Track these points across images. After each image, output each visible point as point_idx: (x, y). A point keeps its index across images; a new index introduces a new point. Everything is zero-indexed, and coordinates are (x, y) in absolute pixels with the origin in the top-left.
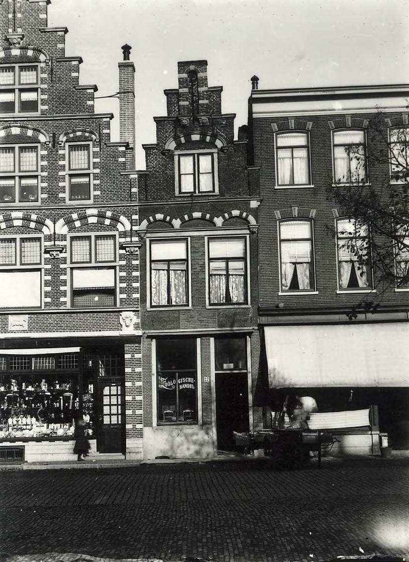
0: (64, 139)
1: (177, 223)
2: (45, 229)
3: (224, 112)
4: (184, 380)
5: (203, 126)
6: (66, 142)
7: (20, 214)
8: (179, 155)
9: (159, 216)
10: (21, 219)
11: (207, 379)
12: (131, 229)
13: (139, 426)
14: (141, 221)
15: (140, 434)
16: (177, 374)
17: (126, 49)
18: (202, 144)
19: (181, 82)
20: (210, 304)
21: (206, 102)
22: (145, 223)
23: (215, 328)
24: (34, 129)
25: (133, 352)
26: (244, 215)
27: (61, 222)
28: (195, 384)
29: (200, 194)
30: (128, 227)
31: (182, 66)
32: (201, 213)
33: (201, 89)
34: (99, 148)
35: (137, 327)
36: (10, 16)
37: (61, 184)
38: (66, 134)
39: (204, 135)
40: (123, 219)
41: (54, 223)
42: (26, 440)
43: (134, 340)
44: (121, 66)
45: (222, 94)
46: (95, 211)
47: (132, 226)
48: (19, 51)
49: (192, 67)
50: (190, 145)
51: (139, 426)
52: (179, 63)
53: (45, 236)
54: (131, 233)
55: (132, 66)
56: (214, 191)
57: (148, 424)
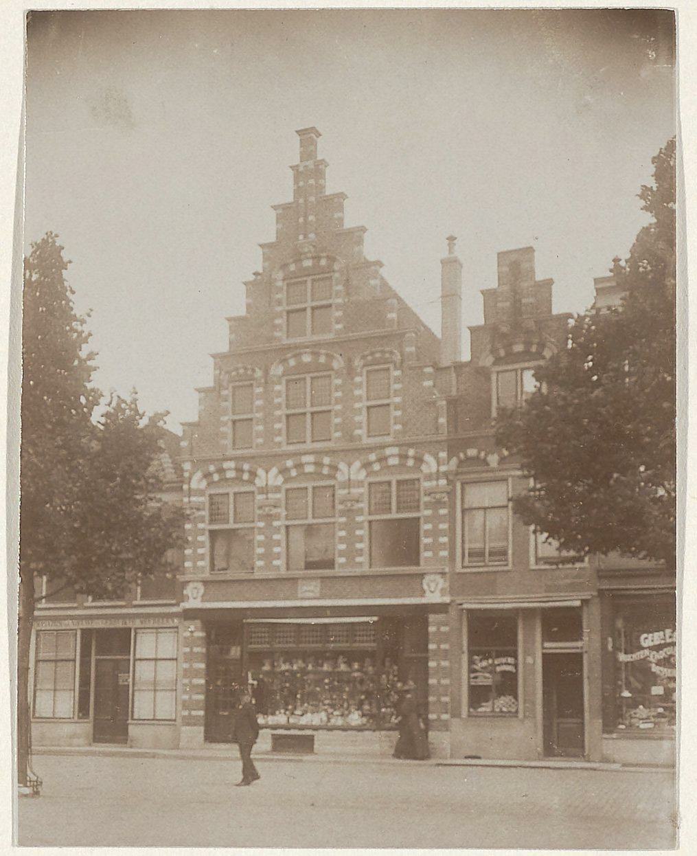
0: (362, 362)
1: (493, 460)
2: (338, 475)
3: (555, 312)
4: (504, 660)
5: (528, 332)
6: (364, 366)
7: (310, 458)
9: (472, 452)
11: (530, 660)
13: (445, 717)
14: (449, 458)
15: (445, 726)
16: (494, 654)
17: (451, 239)
20: (538, 560)
21: (531, 300)
22: (454, 461)
23: (541, 593)
24: (295, 356)
25: (439, 624)
26: (462, 455)
27: (274, 471)
28: (516, 666)
30: (434, 469)
32: (199, 471)
33: (525, 285)
34: (222, 393)
35: (443, 592)
36: (301, 220)
37: (357, 419)
38: (364, 357)
40: (428, 458)
41: (267, 473)
42: (316, 729)
43: (441, 608)
44: (444, 262)
45: (554, 287)
46: (395, 450)
47: (438, 465)
48: (311, 261)
49: (513, 257)
51: (445, 717)
52: (499, 254)
53: (258, 488)
54: (438, 475)
55: (456, 261)
57: (456, 714)
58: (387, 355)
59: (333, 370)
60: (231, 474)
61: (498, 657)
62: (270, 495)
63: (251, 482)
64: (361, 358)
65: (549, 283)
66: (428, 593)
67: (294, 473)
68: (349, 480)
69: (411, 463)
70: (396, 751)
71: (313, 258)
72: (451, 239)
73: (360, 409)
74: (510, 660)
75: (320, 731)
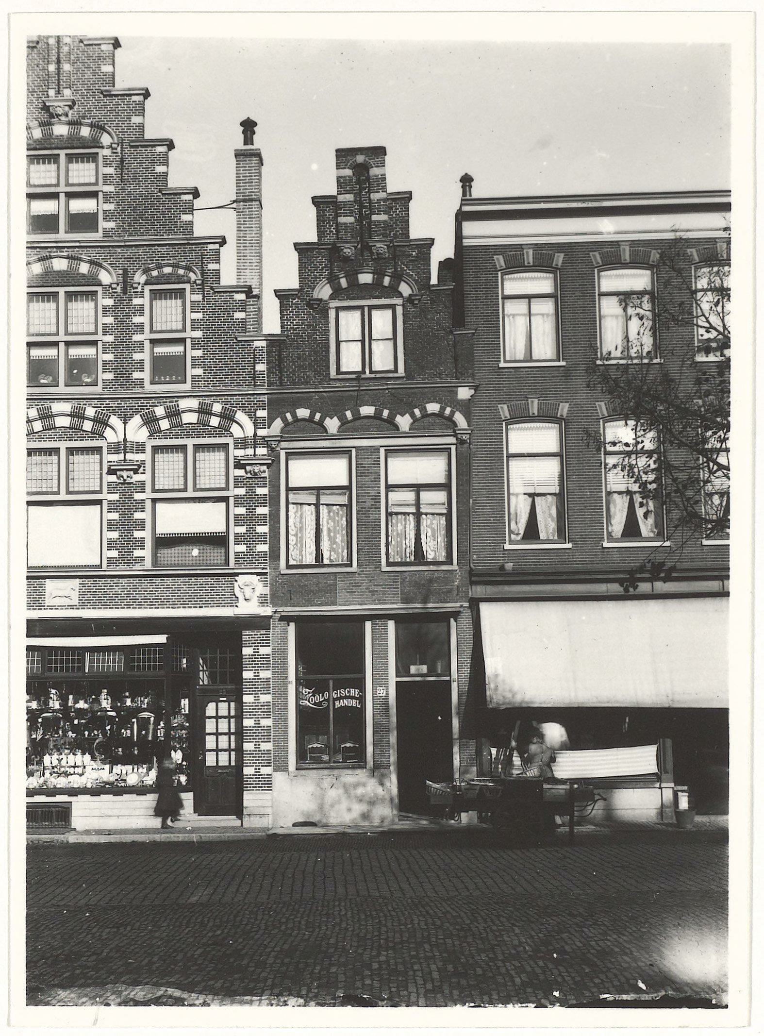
1: (332, 424)
2: (108, 433)
4: (344, 692)
5: (379, 258)
6: (146, 283)
7: (66, 407)
8: (338, 309)
9: (303, 413)
10: (68, 415)
11: (381, 692)
12: (255, 435)
14: (271, 420)
15: (266, 784)
17: (249, 127)
18: (375, 289)
19: (341, 183)
21: (383, 217)
22: (278, 424)
25: (257, 645)
26: (448, 411)
27: (137, 420)
28: (362, 699)
29: (373, 376)
30: (250, 430)
31: (344, 155)
33: (375, 196)
36: (52, 68)
37: (137, 356)
38: (146, 271)
39: (379, 274)
40: (240, 416)
41: (125, 423)
42: (74, 792)
43: (258, 623)
44: (239, 155)
45: (412, 204)
46: (194, 403)
49: (360, 159)
50: (356, 290)
54: (256, 441)
56: (396, 370)
57: (281, 767)
58: (181, 272)
59: (100, 285)
60: (63, 422)
61: (335, 689)
62: (129, 456)
63: (224, 430)
64: (144, 273)
65: (407, 197)
66: (242, 602)
67: (165, 424)
68: (125, 440)
69: (88, 426)
70: (155, 811)
71: (70, 123)
72: (249, 127)
73: (141, 343)
74: (354, 692)
75: (81, 797)
